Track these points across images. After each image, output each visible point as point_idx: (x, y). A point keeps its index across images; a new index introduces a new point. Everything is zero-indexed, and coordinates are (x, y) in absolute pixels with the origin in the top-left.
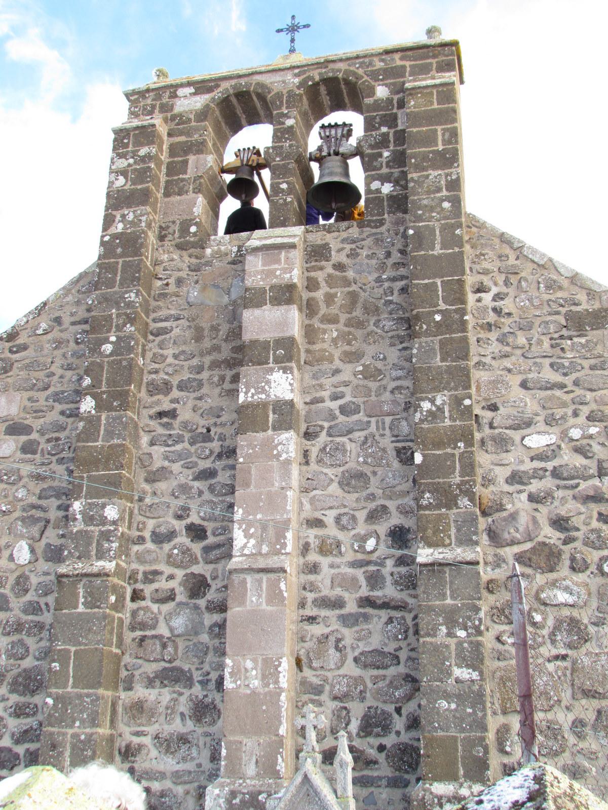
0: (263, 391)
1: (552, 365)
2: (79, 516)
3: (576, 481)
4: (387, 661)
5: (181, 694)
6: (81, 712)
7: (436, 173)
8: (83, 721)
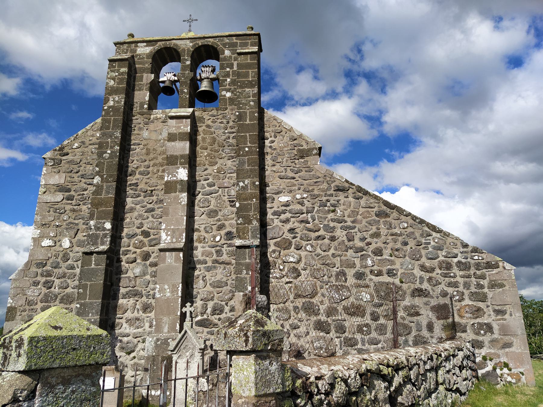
0: (175, 176)
1: (291, 170)
2: (93, 227)
3: (298, 215)
4: (223, 285)
5: (138, 301)
6: (92, 309)
7: (248, 90)
8: (93, 314)
